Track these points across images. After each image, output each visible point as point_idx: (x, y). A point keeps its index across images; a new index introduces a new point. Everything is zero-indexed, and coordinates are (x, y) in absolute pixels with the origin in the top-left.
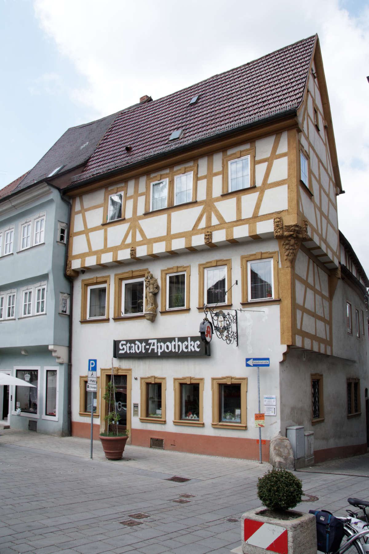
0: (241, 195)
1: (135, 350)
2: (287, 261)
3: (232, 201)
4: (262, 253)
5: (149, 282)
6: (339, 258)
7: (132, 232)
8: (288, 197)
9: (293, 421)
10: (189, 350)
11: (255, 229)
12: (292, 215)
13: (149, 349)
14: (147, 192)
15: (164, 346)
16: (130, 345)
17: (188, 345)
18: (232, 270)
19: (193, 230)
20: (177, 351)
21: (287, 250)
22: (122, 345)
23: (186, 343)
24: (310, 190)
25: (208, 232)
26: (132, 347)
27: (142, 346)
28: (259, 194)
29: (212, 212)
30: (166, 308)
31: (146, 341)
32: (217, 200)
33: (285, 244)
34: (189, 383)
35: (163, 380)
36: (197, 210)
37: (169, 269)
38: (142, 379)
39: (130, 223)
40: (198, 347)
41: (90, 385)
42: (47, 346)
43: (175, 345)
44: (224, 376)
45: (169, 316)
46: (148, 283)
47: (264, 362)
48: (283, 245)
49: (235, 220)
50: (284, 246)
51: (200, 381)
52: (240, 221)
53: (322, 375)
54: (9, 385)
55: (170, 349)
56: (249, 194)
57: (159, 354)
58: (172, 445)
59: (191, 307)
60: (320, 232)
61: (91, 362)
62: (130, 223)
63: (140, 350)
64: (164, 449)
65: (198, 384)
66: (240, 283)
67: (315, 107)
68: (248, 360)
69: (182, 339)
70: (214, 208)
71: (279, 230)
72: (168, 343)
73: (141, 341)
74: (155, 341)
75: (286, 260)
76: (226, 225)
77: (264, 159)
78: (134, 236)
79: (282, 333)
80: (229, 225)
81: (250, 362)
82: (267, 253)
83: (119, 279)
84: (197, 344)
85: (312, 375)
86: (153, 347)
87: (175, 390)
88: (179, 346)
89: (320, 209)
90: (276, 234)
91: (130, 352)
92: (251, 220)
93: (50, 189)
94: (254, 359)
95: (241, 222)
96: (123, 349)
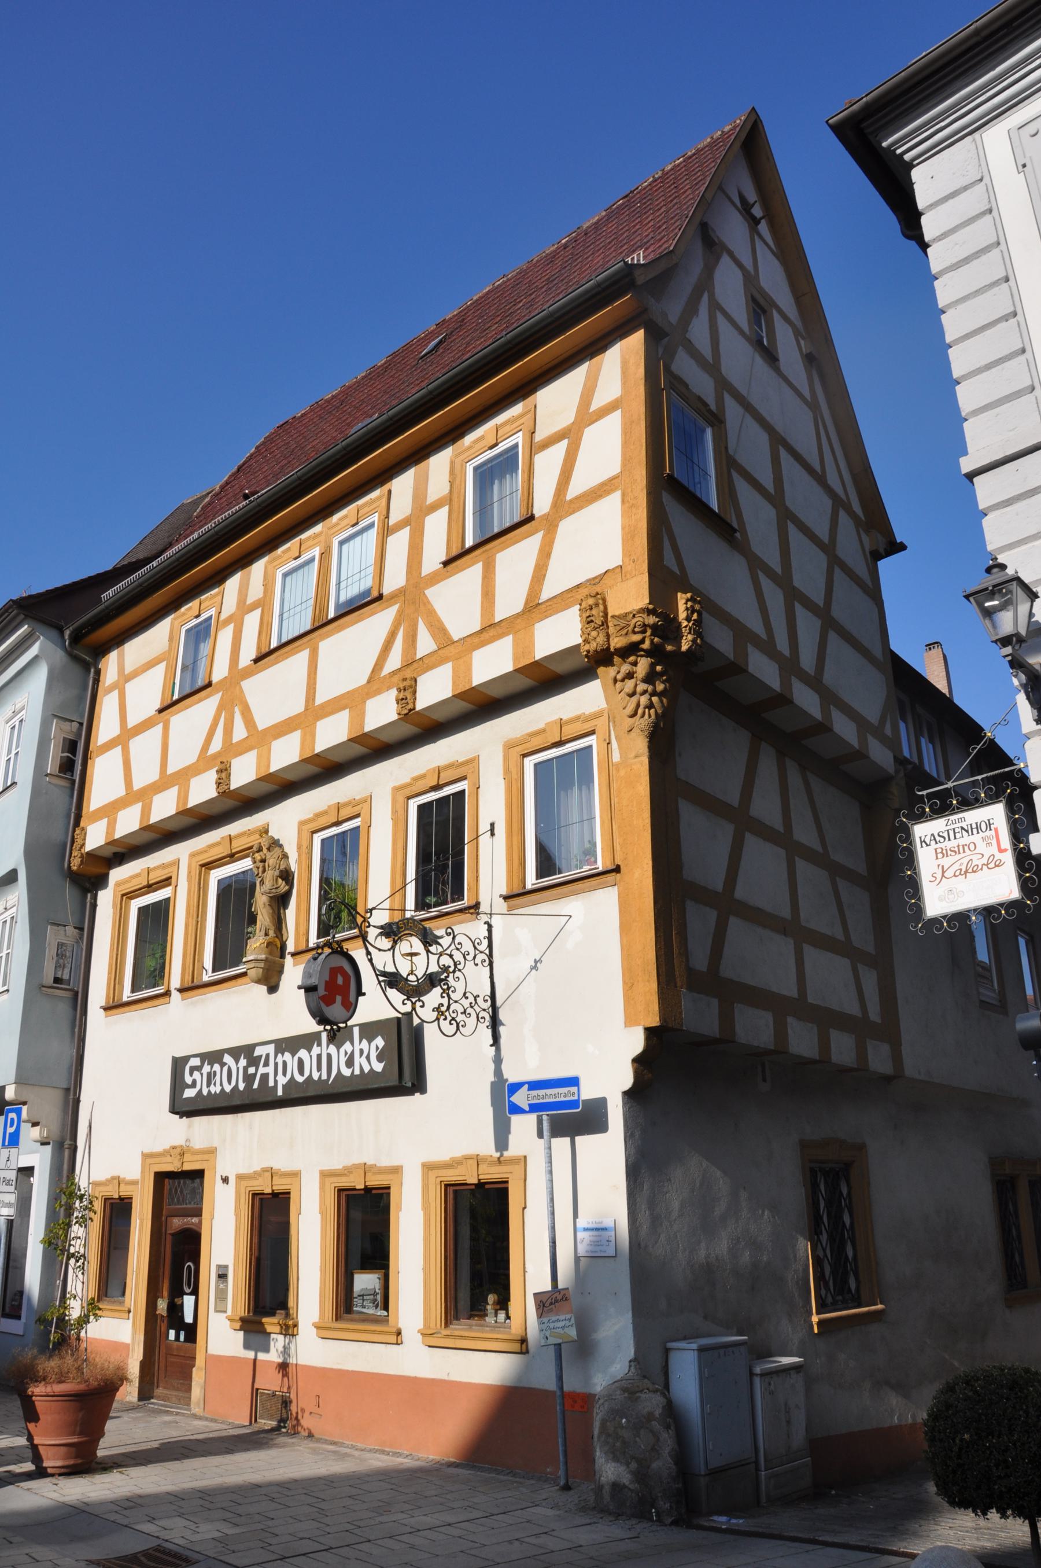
4: (561, 723)
5: (263, 861)
6: (893, 744)
8: (623, 528)
9: (706, 1318)
10: (357, 1072)
12: (634, 579)
13: (255, 1075)
17: (353, 1052)
18: (480, 790)
19: (369, 682)
20: (324, 1077)
21: (632, 695)
22: (193, 1069)
24: (722, 515)
25: (405, 680)
26: (215, 1073)
27: (238, 1069)
29: (420, 619)
30: (307, 941)
31: (246, 1052)
33: (619, 677)
38: (240, 1178)
43: (319, 1057)
44: (458, 1153)
46: (261, 865)
50: (619, 685)
51: (391, 1177)
53: (861, 1148)
60: (782, 644)
63: (307, 1073)
66: (501, 830)
67: (758, 297)
70: (424, 604)
71: (594, 634)
73: (236, 1052)
74: (271, 1049)
76: (452, 650)
77: (559, 431)
85: (804, 1145)
88: (329, 1056)
89: (784, 580)
90: (587, 647)
92: (519, 621)
94: (535, 1085)
95: (492, 632)
96: (194, 1084)
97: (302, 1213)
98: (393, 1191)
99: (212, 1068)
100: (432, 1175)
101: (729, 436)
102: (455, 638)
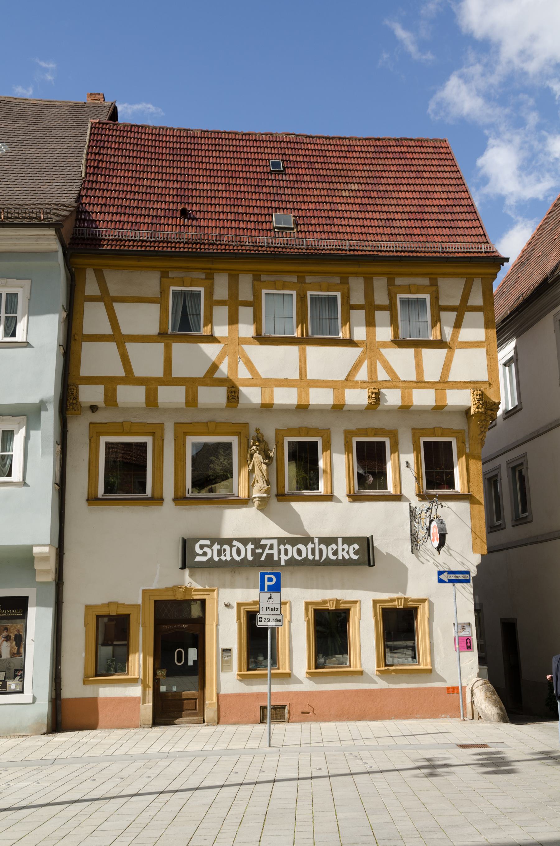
1: (231, 555)
11: (444, 397)
13: (261, 554)
14: (161, 297)
15: (292, 551)
16: (219, 547)
17: (337, 550)
20: (317, 558)
23: (334, 546)
25: (374, 389)
26: (225, 550)
27: (246, 550)
29: (378, 361)
31: (256, 542)
38: (239, 605)
40: (356, 553)
41: (264, 617)
43: (313, 550)
49: (437, 379)
52: (420, 383)
55: (304, 555)
57: (283, 563)
58: (302, 713)
63: (243, 556)
65: (416, 609)
66: (403, 465)
68: (440, 573)
72: (301, 546)
73: (244, 541)
74: (275, 542)
78: (372, 370)
80: (406, 384)
84: (354, 549)
86: (271, 552)
88: (321, 551)
91: (220, 560)
94: (450, 572)
95: (423, 385)
97: (220, 623)
99: (221, 547)
101: (88, 431)
102: (426, 379)
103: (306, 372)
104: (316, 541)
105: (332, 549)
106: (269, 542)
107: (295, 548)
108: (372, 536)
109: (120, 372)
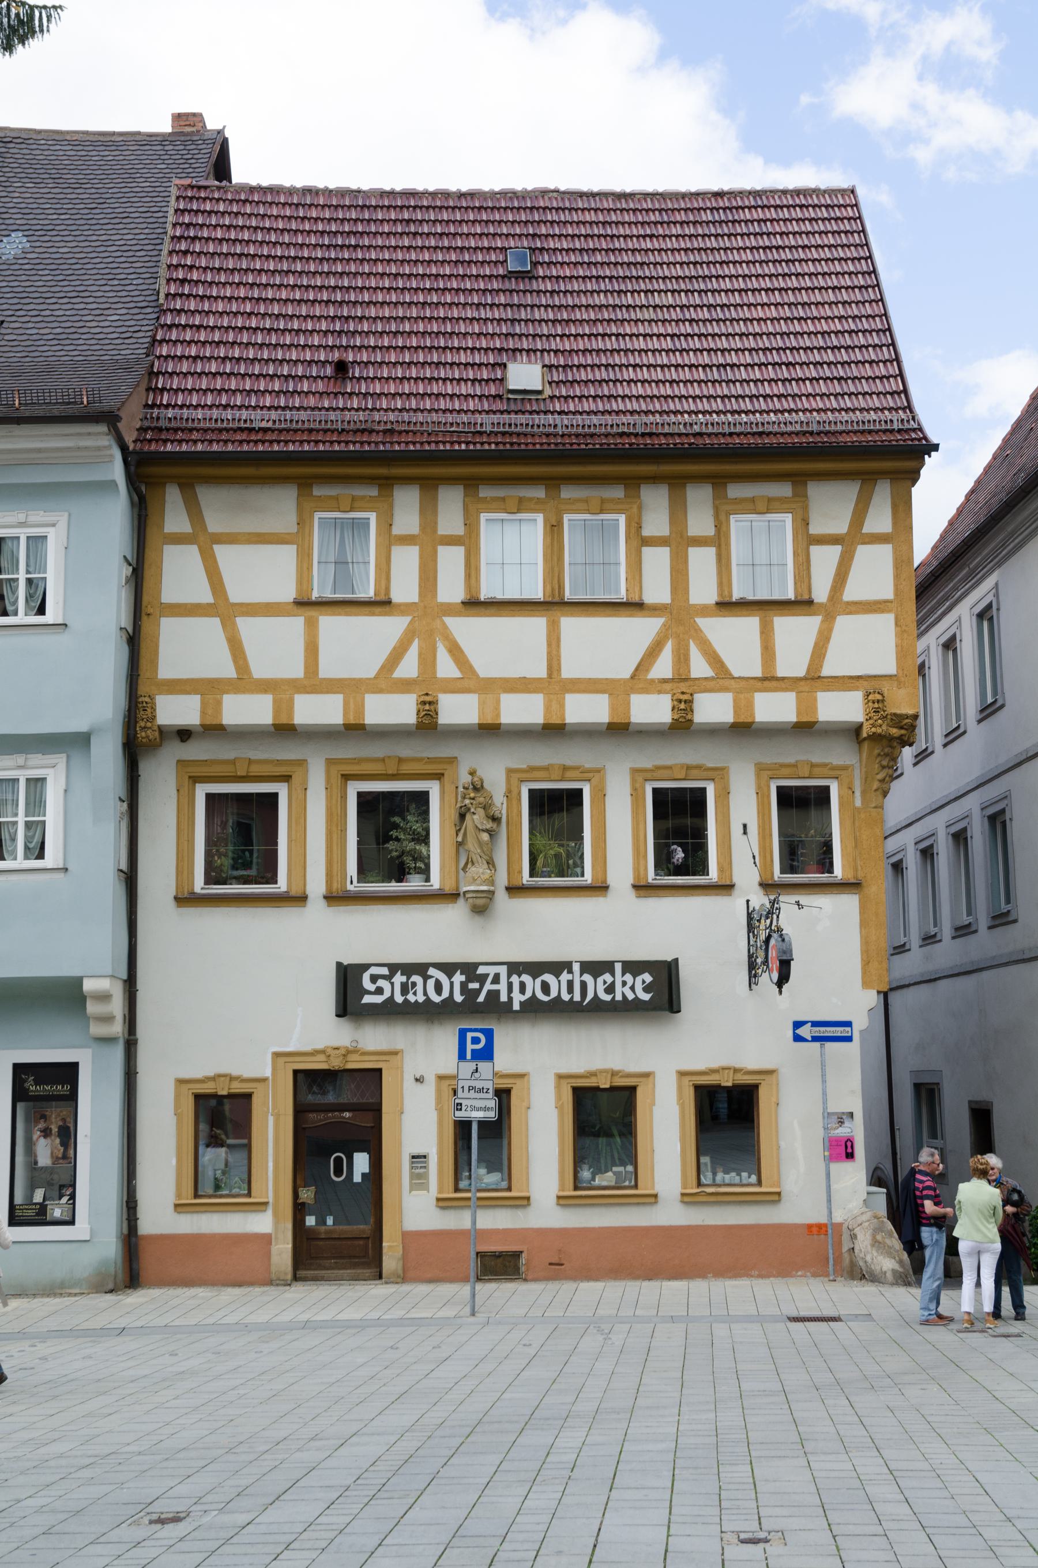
0: (771, 613)
1: (425, 993)
2: (878, 793)
3: (750, 624)
4: (813, 766)
7: (420, 648)
13: (478, 991)
15: (533, 986)
16: (404, 979)
17: (613, 983)
19: (633, 677)
20: (577, 997)
21: (883, 767)
25: (683, 693)
26: (414, 984)
27: (452, 984)
28: (822, 622)
31: (469, 969)
32: (704, 611)
34: (607, 1086)
35: (518, 1081)
36: (646, 628)
37: (532, 769)
39: (408, 619)
40: (646, 990)
41: (464, 1102)
42: (78, 981)
43: (570, 984)
44: (715, 1065)
45: (521, 900)
47: (838, 1031)
48: (879, 755)
49: (759, 674)
52: (770, 681)
54: (970, 1102)
55: (554, 994)
56: (793, 615)
57: (516, 1006)
58: (551, 1264)
59: (611, 880)
61: (470, 1035)
62: (408, 619)
63: (445, 994)
64: (525, 1280)
65: (755, 1087)
66: (736, 830)
69: (595, 968)
71: (880, 721)
72: (548, 978)
73: (449, 969)
74: (503, 970)
75: (876, 790)
79: (866, 963)
80: (743, 684)
81: (805, 1031)
82: (825, 765)
83: (342, 775)
84: (644, 982)
86: (495, 987)
87: (560, 1108)
88: (584, 985)
93: (109, 447)
94: (815, 1024)
95: (774, 684)
98: (763, 1093)
99: (408, 979)
100: (185, 1087)
103: (559, 664)
104: (576, 967)
105: (605, 982)
106: (492, 970)
107: (538, 981)
108: (676, 960)
109: (229, 671)
